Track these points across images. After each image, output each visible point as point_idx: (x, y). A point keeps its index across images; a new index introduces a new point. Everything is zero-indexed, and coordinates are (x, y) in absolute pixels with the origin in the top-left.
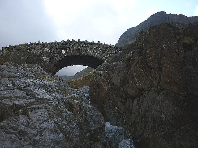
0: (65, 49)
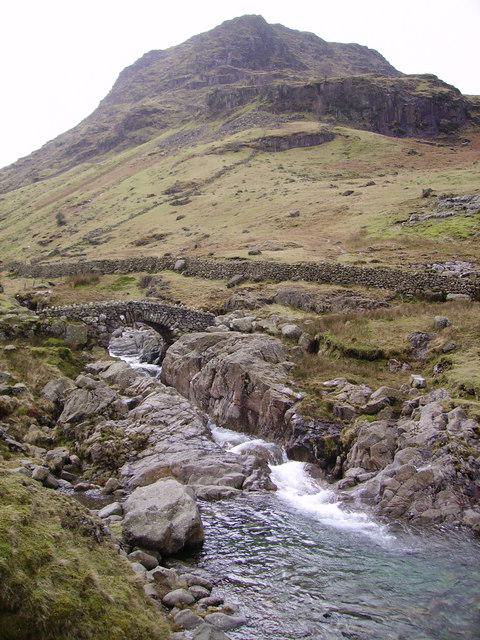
0: (124, 313)
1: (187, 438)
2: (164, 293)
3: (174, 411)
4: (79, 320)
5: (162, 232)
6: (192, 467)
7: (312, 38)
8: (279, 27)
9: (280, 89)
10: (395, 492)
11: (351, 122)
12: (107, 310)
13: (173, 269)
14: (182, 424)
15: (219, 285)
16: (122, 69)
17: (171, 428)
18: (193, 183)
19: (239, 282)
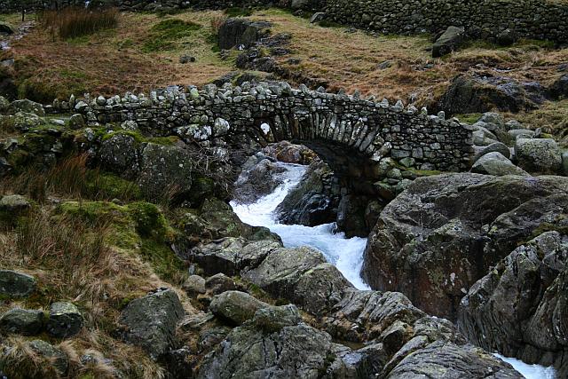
0: (269, 118)
2: (281, 62)
4: (168, 130)
16: (251, 206)
19: (460, 43)
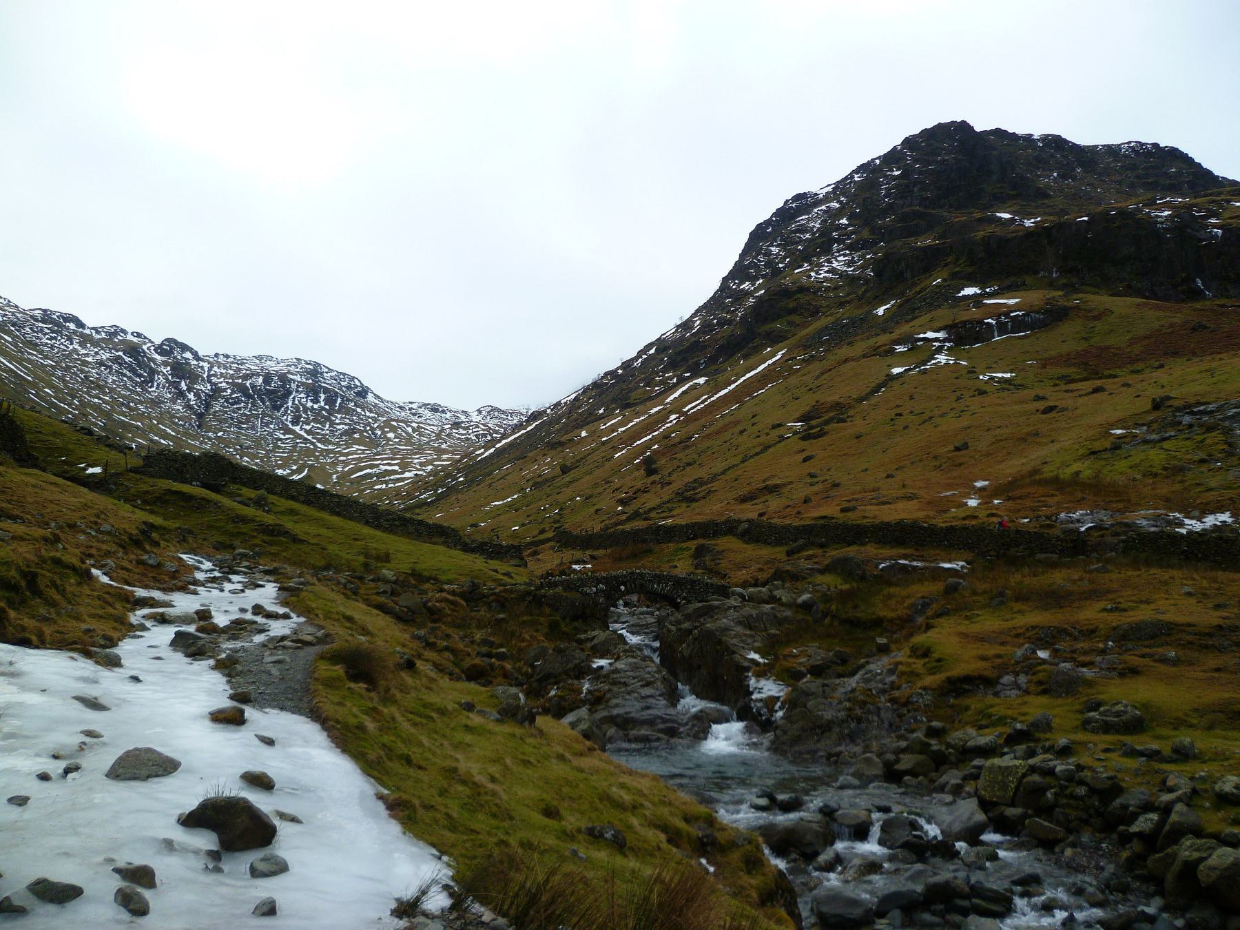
0: (624, 584)
1: (643, 698)
3: (637, 674)
5: (779, 482)
6: (632, 718)
7: (1056, 143)
8: (999, 133)
9: (986, 241)
10: (785, 732)
11: (1106, 284)
12: (606, 581)
13: (735, 535)
14: (641, 686)
15: (779, 552)
16: (753, 228)
17: (629, 688)
18: (838, 404)
